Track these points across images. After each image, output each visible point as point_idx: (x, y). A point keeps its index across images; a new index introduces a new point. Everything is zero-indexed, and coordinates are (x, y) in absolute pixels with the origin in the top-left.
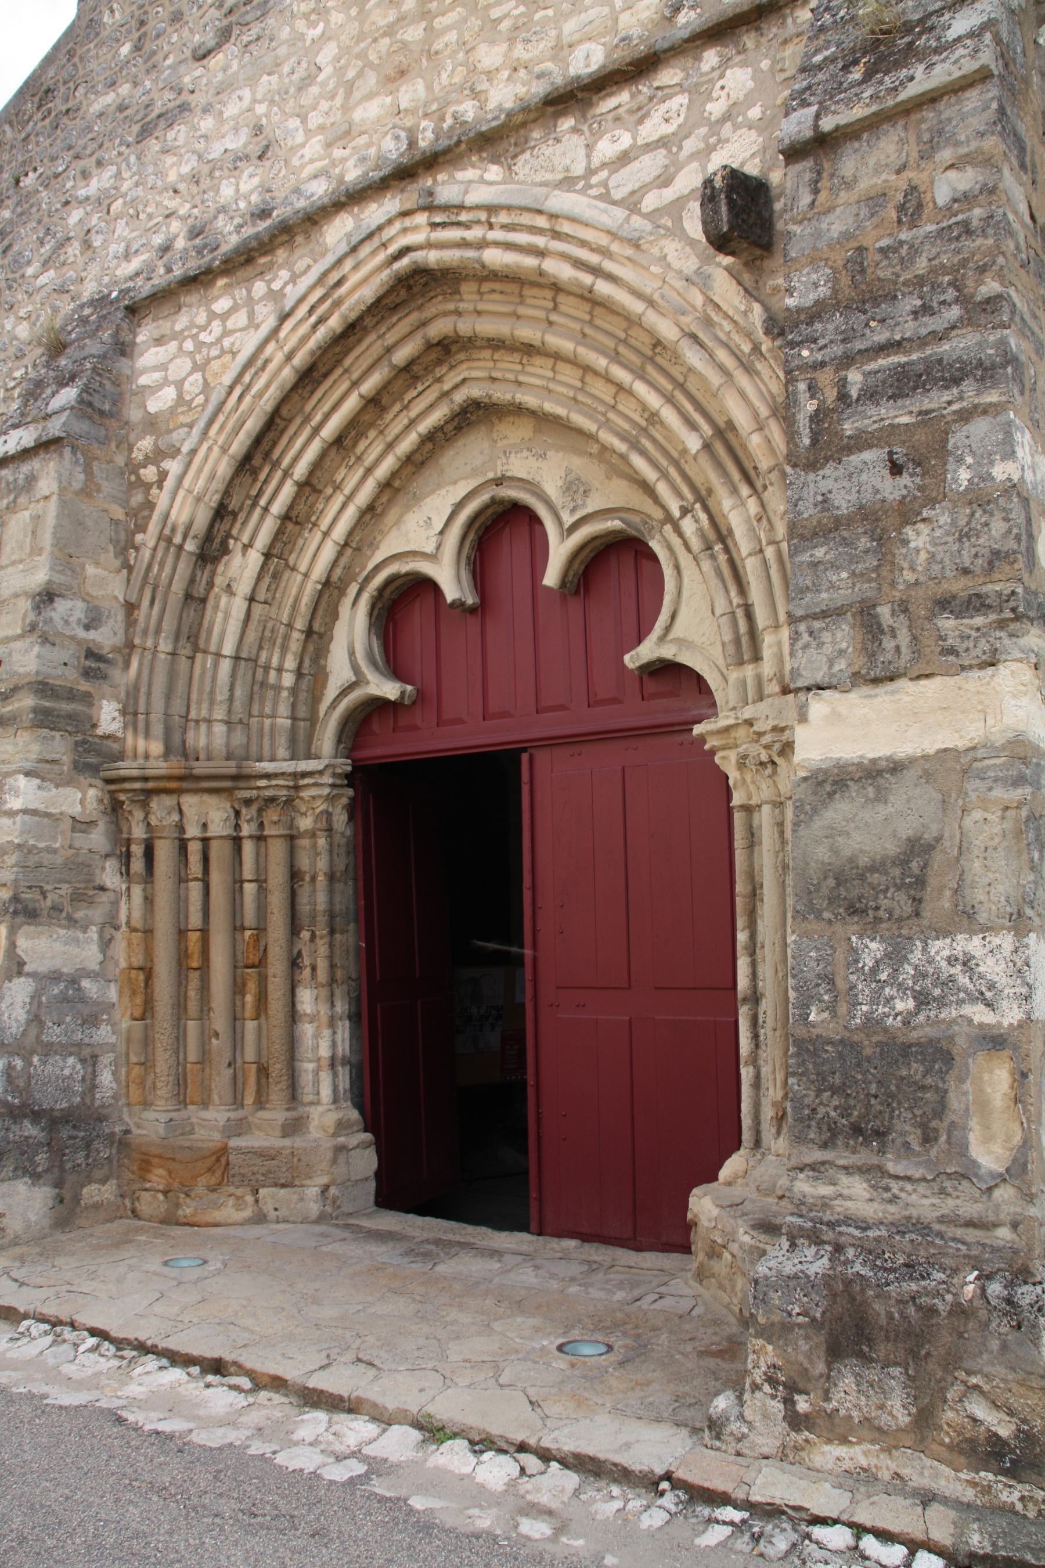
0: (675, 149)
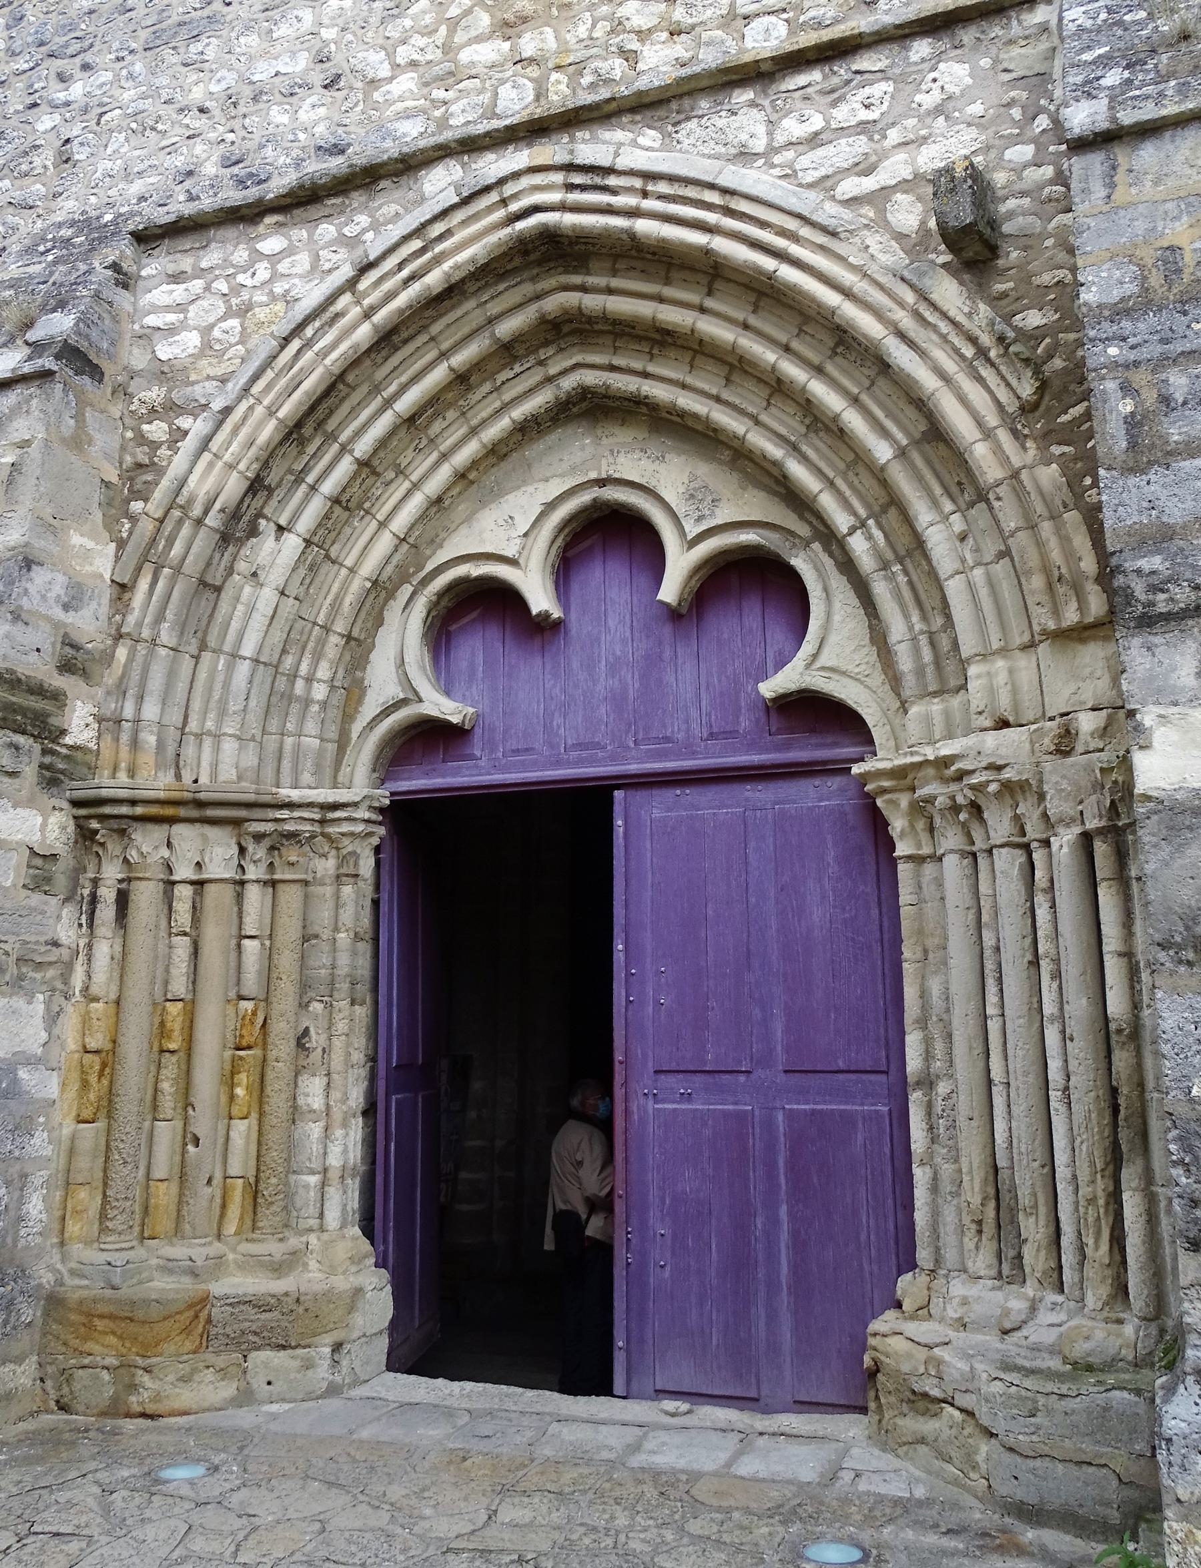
0: (877, 137)
